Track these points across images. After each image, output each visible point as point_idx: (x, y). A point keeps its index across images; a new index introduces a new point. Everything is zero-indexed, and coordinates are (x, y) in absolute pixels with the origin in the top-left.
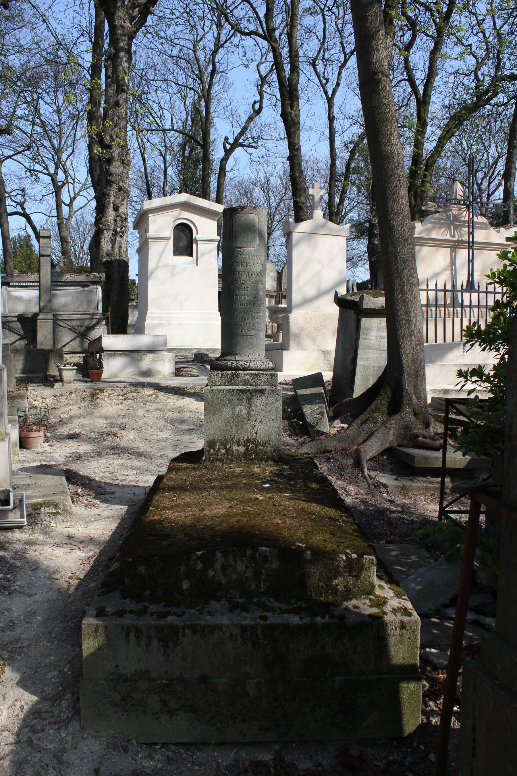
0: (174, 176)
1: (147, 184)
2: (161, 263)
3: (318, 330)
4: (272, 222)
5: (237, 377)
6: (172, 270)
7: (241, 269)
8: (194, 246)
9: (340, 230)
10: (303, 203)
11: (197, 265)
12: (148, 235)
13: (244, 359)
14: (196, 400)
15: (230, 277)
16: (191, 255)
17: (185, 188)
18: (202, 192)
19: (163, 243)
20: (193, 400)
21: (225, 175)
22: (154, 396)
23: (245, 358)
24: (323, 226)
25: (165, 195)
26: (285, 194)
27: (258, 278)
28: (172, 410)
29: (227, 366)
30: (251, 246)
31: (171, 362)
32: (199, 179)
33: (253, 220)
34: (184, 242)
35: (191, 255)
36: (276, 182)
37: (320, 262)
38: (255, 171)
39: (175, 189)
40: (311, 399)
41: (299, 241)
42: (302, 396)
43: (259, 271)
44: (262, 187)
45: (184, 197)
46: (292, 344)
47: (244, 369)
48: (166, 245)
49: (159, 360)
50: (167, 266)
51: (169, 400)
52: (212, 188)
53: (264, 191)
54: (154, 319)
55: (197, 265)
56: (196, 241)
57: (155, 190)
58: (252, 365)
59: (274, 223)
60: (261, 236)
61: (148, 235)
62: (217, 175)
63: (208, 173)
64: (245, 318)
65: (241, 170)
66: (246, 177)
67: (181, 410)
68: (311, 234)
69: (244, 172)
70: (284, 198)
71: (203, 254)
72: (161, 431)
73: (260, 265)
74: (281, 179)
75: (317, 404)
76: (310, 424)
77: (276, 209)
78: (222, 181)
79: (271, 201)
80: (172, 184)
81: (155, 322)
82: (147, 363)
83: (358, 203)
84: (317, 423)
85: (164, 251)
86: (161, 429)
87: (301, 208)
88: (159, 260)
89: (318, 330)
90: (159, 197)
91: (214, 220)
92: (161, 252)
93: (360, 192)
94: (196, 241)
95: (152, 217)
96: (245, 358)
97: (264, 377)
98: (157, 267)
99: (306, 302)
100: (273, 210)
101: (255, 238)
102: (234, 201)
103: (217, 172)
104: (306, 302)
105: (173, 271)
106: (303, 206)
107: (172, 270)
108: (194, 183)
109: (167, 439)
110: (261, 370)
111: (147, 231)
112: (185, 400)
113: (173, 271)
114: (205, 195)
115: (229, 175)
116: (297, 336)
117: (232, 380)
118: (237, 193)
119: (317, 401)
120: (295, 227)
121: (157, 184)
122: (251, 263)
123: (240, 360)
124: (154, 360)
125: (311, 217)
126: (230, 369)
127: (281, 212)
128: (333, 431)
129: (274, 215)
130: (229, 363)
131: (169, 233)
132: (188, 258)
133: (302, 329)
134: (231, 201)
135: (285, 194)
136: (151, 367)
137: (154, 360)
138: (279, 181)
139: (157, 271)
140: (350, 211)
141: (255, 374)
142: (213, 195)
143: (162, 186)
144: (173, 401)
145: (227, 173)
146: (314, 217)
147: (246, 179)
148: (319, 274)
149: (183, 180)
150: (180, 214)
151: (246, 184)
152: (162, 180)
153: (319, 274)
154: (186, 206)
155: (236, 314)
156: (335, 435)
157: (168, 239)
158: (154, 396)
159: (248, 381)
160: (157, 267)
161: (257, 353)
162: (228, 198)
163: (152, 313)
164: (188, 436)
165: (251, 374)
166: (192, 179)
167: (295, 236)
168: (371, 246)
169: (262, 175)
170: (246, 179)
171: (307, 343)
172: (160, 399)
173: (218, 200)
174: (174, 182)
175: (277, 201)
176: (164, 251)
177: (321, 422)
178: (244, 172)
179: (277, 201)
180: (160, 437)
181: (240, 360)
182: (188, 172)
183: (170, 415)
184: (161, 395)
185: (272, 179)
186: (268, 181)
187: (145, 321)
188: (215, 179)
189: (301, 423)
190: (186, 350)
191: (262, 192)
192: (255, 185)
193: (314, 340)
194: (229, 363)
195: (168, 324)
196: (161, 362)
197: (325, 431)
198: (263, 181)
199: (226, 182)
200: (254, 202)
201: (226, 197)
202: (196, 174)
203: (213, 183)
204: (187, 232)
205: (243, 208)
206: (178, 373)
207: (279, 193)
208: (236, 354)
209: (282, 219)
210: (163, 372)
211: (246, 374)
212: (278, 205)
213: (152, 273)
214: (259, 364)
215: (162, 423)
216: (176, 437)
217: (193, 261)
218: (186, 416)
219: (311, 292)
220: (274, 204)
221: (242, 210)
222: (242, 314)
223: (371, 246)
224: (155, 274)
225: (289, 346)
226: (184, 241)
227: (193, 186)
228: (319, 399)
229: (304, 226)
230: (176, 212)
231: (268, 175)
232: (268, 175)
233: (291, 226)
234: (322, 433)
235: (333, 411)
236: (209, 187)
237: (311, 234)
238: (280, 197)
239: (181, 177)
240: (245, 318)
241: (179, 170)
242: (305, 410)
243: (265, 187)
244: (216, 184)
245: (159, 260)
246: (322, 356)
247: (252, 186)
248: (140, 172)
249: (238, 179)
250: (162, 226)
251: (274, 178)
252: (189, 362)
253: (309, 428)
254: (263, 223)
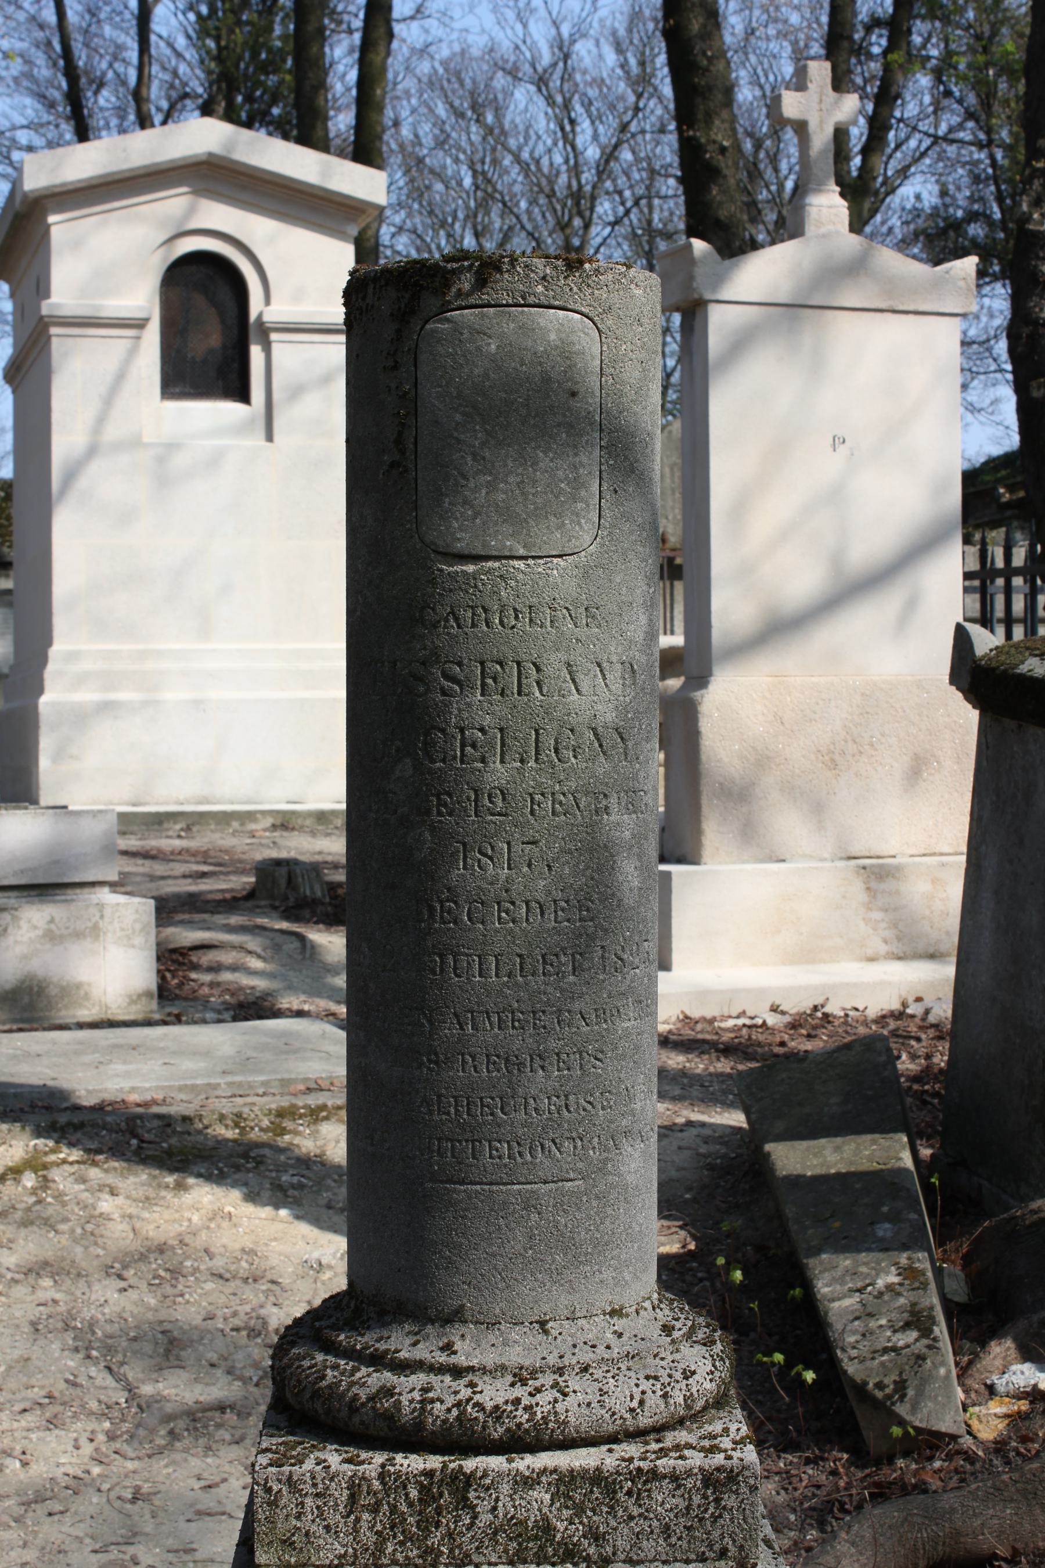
0: (181, 42)
1: (71, 71)
2: (112, 432)
3: (833, 765)
4: (587, 226)
5: (463, 1502)
6: (161, 460)
7: (480, 710)
8: (256, 352)
9: (936, 286)
10: (723, 150)
11: (270, 438)
12: (46, 308)
13: (515, 1356)
14: (252, 1197)
15: (405, 769)
16: (244, 396)
17: (231, 94)
18: (297, 105)
19: (117, 344)
20: (229, 1199)
21: (390, 35)
22: (29, 1180)
23: (520, 1348)
24: (854, 268)
25: (144, 122)
26: (637, 109)
27: (602, 766)
28: (117, 1269)
29: (390, 1417)
30: (556, 541)
31: (138, 940)
32: (282, 54)
33: (567, 353)
34: (210, 339)
35: (244, 396)
36: (597, 59)
37: (838, 441)
38: (511, 15)
39: (186, 96)
40: (855, 1211)
41: (743, 342)
42: (796, 1182)
43: (608, 715)
44: (541, 82)
45: (203, 135)
46: (715, 834)
47: (516, 1444)
48: (132, 353)
49: (78, 935)
50: (135, 443)
51: (106, 1204)
52: (339, 88)
53: (550, 100)
54: (80, 681)
55: (270, 438)
56: (264, 332)
57: (103, 102)
58: (576, 1407)
59: (594, 230)
60: (621, 453)
61: (46, 308)
62: (357, 37)
63: (322, 29)
64: (513, 1063)
65: (457, 13)
66: (477, 43)
67: (163, 1262)
68: (796, 309)
69: (470, 21)
70: (633, 127)
71: (297, 391)
72: (53, 1423)
73: (615, 676)
74: (619, 49)
75: (885, 1247)
76: (860, 1389)
77: (600, 173)
78: (377, 59)
79: (580, 141)
80: (175, 73)
81: (87, 696)
82: (19, 950)
83: (936, 139)
84: (901, 1386)
85: (121, 377)
86: (52, 1408)
87: (713, 173)
88: (101, 421)
89: (833, 765)
90: (122, 131)
91: (339, 234)
92: (109, 388)
93: (948, 93)
94: (264, 332)
95: (61, 227)
96: (520, 1348)
97: (663, 1500)
98: (92, 451)
99: (779, 628)
100: (588, 177)
101: (577, 484)
102: (428, 141)
103: (358, 23)
104: (779, 628)
105: (164, 468)
106: (721, 161)
107: (161, 460)
108: (265, 68)
109: (77, 1485)
110: (638, 1434)
111: (42, 289)
112: (188, 1198)
113: (164, 468)
114: (306, 129)
115: (407, 34)
116: (740, 795)
117: (426, 1525)
118: (441, 110)
119: (884, 1230)
120: (719, 280)
121: (110, 75)
122: (554, 662)
123: (483, 1366)
124: (52, 937)
125: (788, 226)
126: (413, 1439)
127: (622, 181)
128: (989, 1421)
129: (593, 198)
130: (409, 1387)
131: (141, 296)
132: (229, 409)
133: (763, 760)
134: (417, 141)
135: (637, 109)
136: (38, 966)
137: (52, 937)
138: (611, 57)
139: (95, 467)
140: (904, 173)
141: (596, 1477)
142: (342, 122)
143: (133, 79)
144: (127, 1204)
145: (397, 28)
146: (810, 229)
147: (475, 52)
148: (835, 496)
149: (219, 59)
150: (191, 211)
151: (476, 72)
152: (133, 56)
153: (835, 496)
154: (215, 176)
155: (449, 1030)
156: (999, 1446)
157: (140, 324)
158: (29, 1180)
159: (547, 1528)
160: (92, 451)
161: (604, 1300)
162: (405, 132)
163: (73, 656)
164: (195, 1464)
165: (565, 1483)
166: (255, 54)
167: (721, 322)
168: (1026, 331)
169: (541, 34)
170: (475, 52)
171: (788, 825)
172: (59, 1196)
173: (364, 150)
174: (183, 69)
175: (603, 140)
176: (121, 377)
177: (924, 1381)
178: (470, 21)
179: (603, 140)
180: (39, 1470)
181: (483, 1366)
182: (239, 23)
183: (109, 1302)
184: (72, 1174)
185: (583, 50)
186: (566, 57)
187: (40, 690)
188: (351, 51)
189: (810, 1376)
190: (224, 818)
191: (541, 102)
192: (513, 73)
193: (817, 810)
194: (409, 1387)
195: (145, 704)
196: (87, 944)
197: (946, 1424)
198: (546, 59)
199: (395, 65)
200: (512, 143)
201: (396, 124)
202: (270, 29)
203: (341, 68)
204: (225, 294)
205: (487, 268)
206: (178, 990)
207: (612, 107)
208: (455, 1317)
209: (627, 212)
210: (96, 993)
211: (526, 1482)
212: (610, 155)
213: (70, 476)
214: (622, 1394)
215: (58, 1360)
216: (129, 1468)
217: (252, 421)
218: (196, 1304)
219: (800, 580)
220: (592, 153)
221: (481, 282)
222: (490, 1034)
223: (1026, 331)
224: (82, 482)
225: (698, 845)
226: (209, 331)
227: (258, 84)
228: (894, 1218)
229: (765, 272)
230: (172, 204)
231: (566, 30)
232: (566, 30)
233: (699, 271)
234: (932, 1442)
235: (967, 1261)
236: (322, 85)
237: (796, 309)
238: (615, 124)
239: (211, 44)
240: (513, 1063)
241: (199, 15)
242: (823, 1288)
243: (555, 82)
244: (353, 75)
245: (101, 421)
246: (857, 889)
247: (501, 80)
248: (42, 27)
249: (445, 52)
250: (107, 266)
251: (590, 44)
252: (230, 904)
253: (860, 1412)
254: (631, 373)
